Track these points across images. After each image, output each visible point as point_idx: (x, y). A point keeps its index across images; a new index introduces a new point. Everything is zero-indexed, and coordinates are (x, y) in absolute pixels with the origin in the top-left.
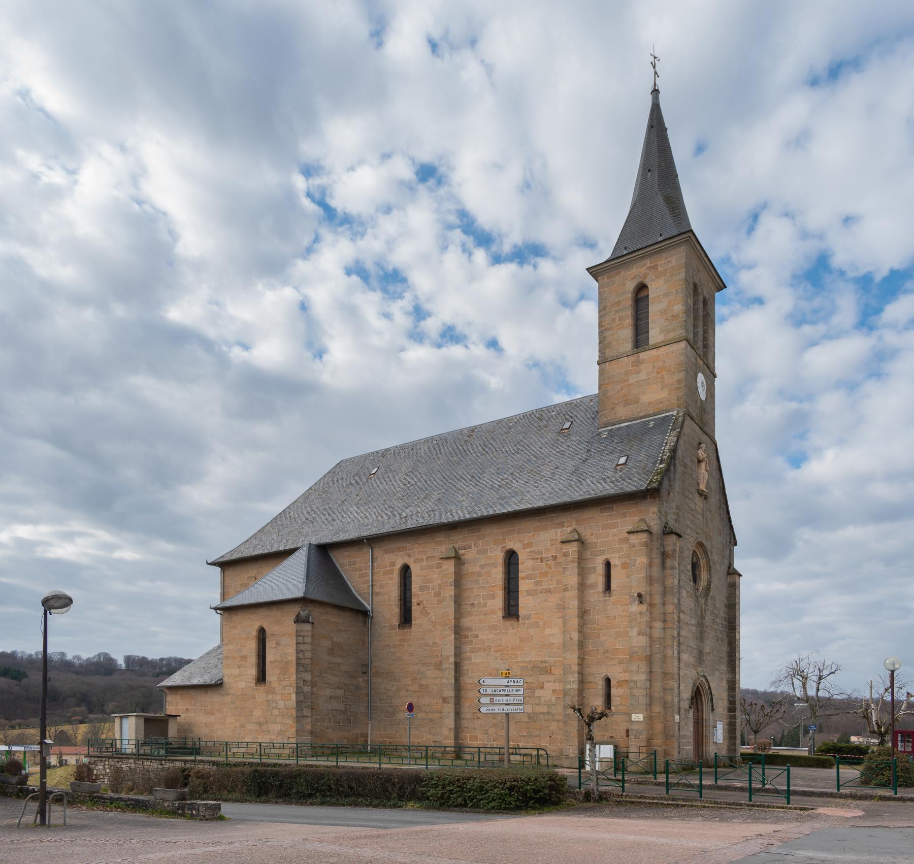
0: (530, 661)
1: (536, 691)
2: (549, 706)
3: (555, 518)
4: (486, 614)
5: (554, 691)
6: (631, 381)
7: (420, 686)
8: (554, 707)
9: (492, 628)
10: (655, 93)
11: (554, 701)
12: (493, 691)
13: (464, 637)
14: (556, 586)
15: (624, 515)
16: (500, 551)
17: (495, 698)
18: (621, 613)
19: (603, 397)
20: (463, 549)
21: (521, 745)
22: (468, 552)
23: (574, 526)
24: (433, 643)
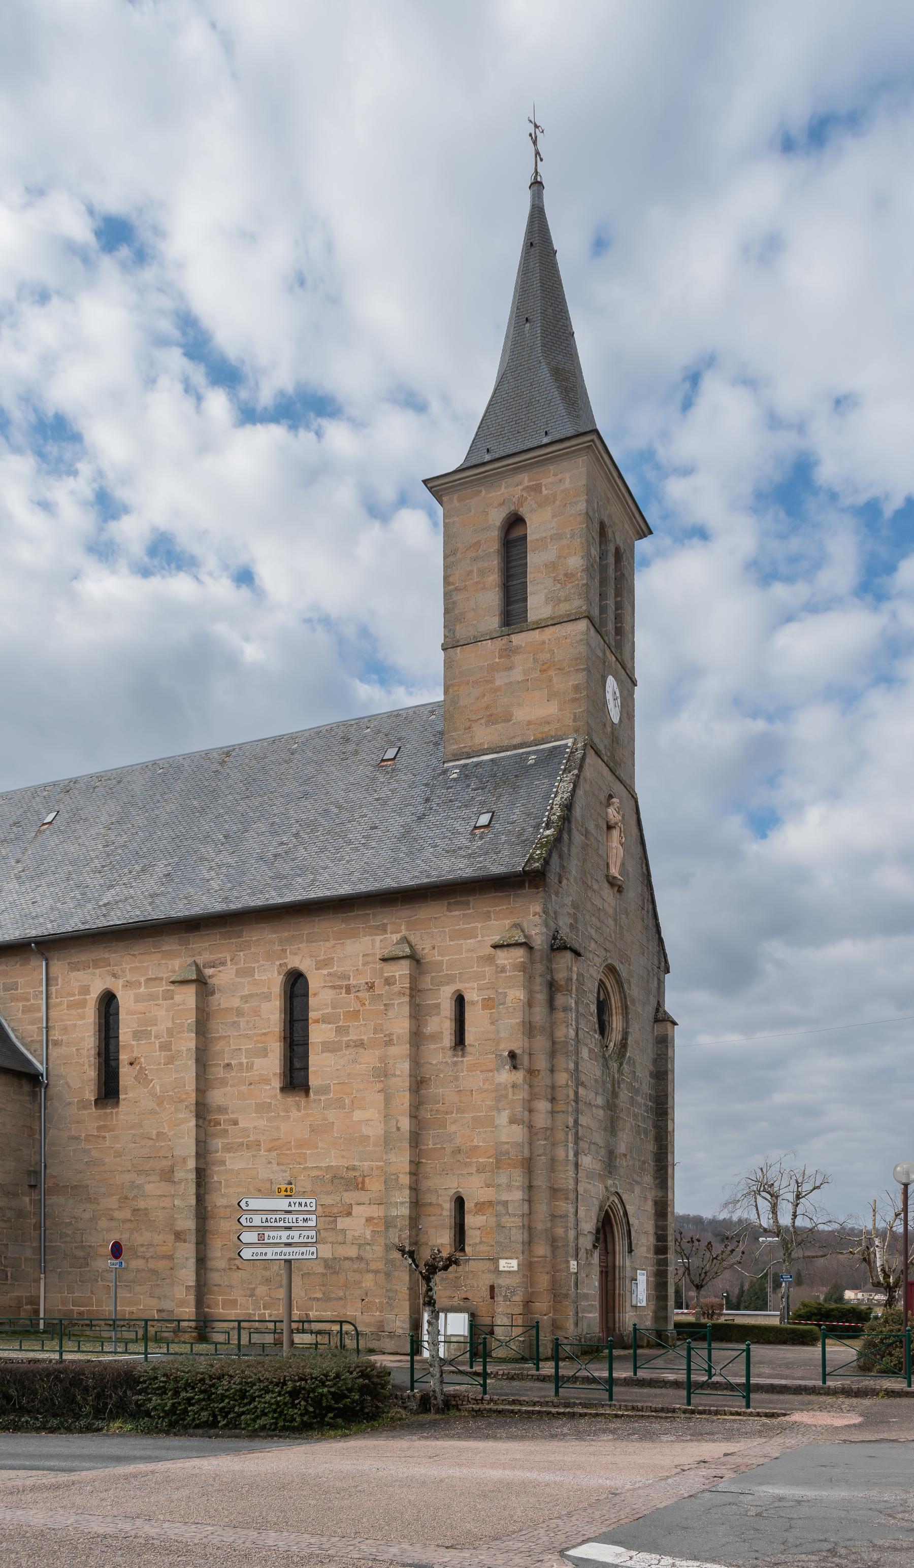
2: (360, 1246)
4: (251, 1084)
5: (369, 1220)
8: (368, 1247)
9: (263, 1108)
10: (535, 187)
11: (368, 1237)
13: (212, 1124)
14: (372, 1035)
15: (487, 916)
16: (276, 971)
17: (266, 1234)
19: (451, 708)
20: (211, 967)
22: (220, 971)
23: (404, 932)
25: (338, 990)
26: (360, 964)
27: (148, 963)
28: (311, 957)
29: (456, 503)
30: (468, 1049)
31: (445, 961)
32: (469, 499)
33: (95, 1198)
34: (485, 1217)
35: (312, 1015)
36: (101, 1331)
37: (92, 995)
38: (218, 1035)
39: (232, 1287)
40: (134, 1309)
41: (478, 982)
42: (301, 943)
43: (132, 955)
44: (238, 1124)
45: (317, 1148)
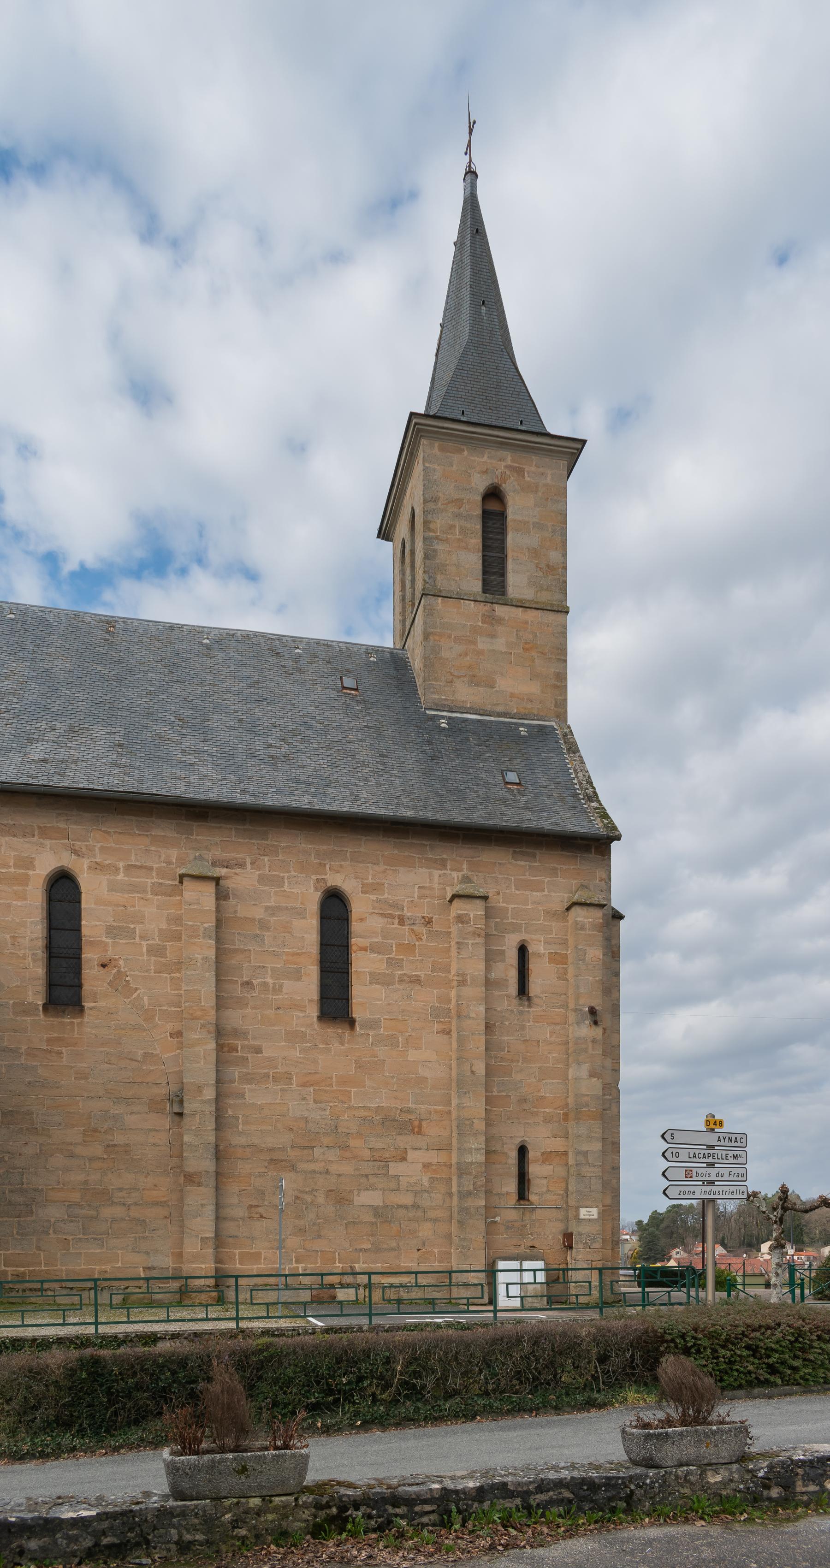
0: (378, 1109)
1: (390, 1164)
2: (416, 1193)
3: (428, 848)
4: (279, 1008)
5: (426, 1166)
6: (481, 646)
7: (108, 1146)
8: (426, 1194)
9: (293, 1037)
10: (469, 177)
11: (426, 1184)
12: (691, 1156)
13: (226, 1049)
14: (430, 973)
15: (554, 872)
16: (312, 885)
17: (694, 1170)
18: (548, 1036)
19: (432, 656)
20: (223, 866)
21: (358, 1267)
22: (236, 874)
23: (465, 872)
24: (146, 1055)
25: (389, 920)
26: (416, 897)
27: (130, 847)
28: (356, 878)
29: (436, 450)
30: (535, 1000)
31: (510, 909)
32: (450, 452)
33: (43, 1129)
34: (551, 1167)
35: (355, 941)
36: (55, 1296)
37: (37, 871)
38: (233, 947)
39: (253, 1238)
40: (108, 1267)
41: (544, 935)
42: (345, 860)
43: (104, 832)
44: (262, 1053)
45: (364, 1086)
